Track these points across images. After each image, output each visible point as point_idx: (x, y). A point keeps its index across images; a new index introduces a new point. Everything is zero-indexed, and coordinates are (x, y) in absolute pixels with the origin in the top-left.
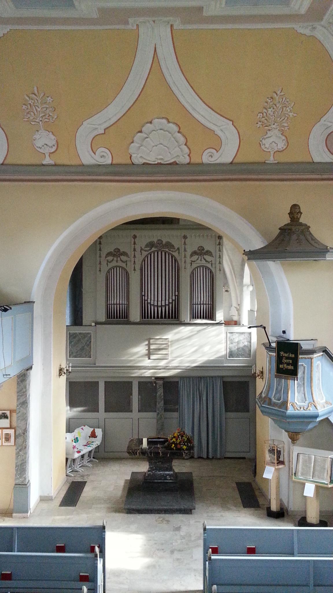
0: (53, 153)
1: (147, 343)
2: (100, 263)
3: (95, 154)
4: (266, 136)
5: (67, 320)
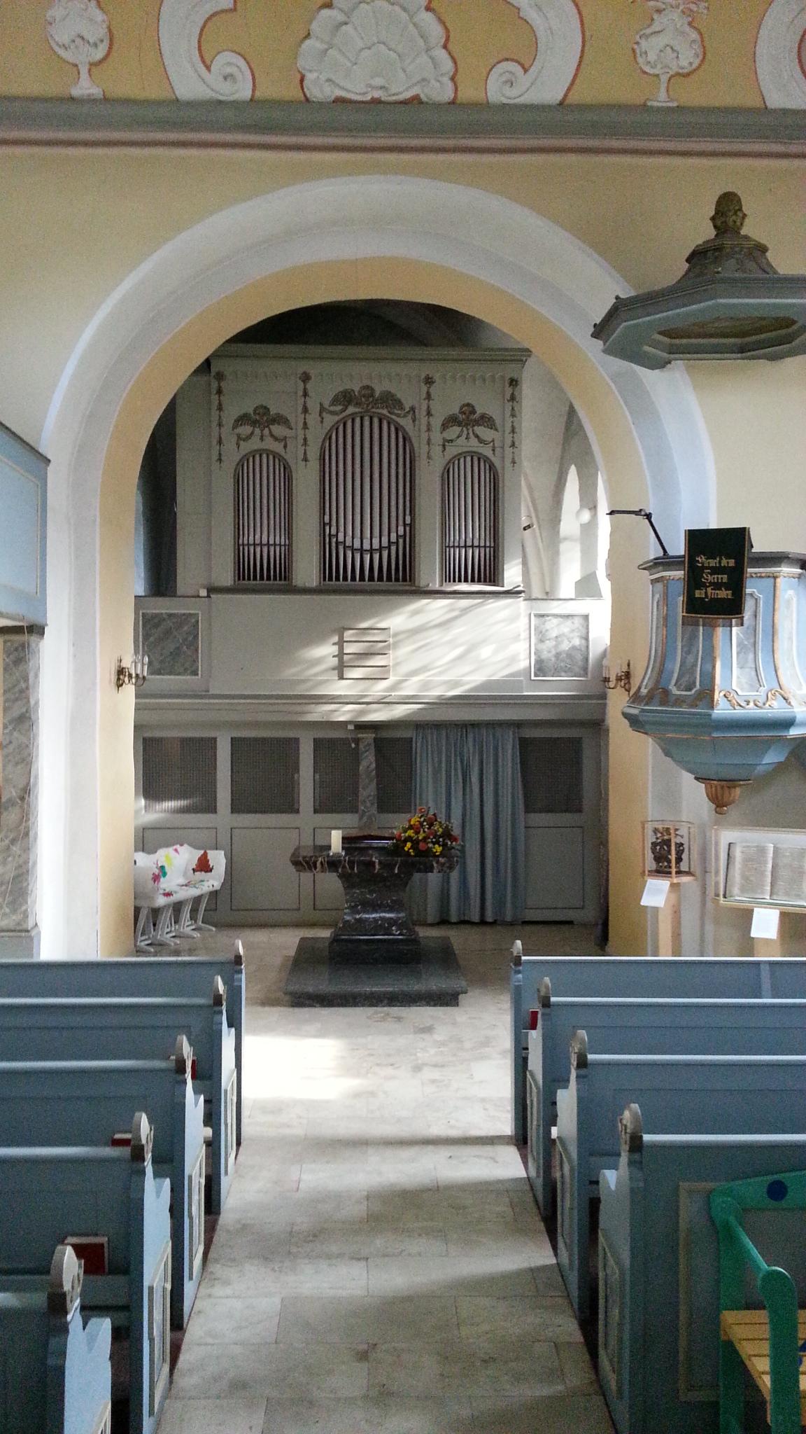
0: (101, 62)
1: (336, 639)
2: (220, 442)
3: (208, 68)
4: (648, 31)
5: (138, 584)
